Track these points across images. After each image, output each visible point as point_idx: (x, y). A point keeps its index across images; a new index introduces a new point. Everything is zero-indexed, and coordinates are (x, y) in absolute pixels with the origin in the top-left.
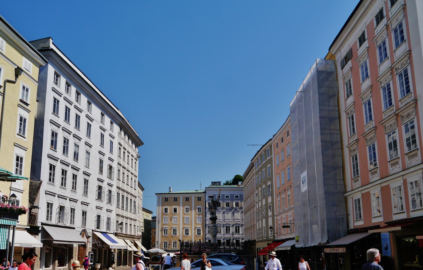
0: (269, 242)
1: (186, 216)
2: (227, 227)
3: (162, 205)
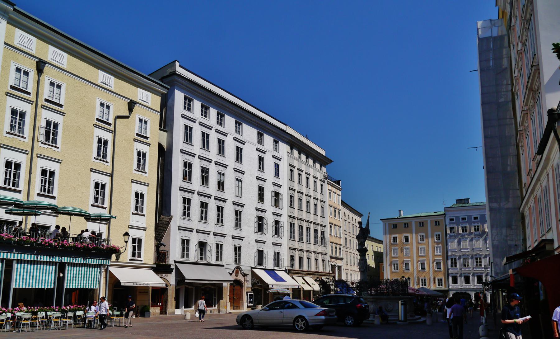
1: (420, 246)
2: (477, 259)
3: (390, 234)
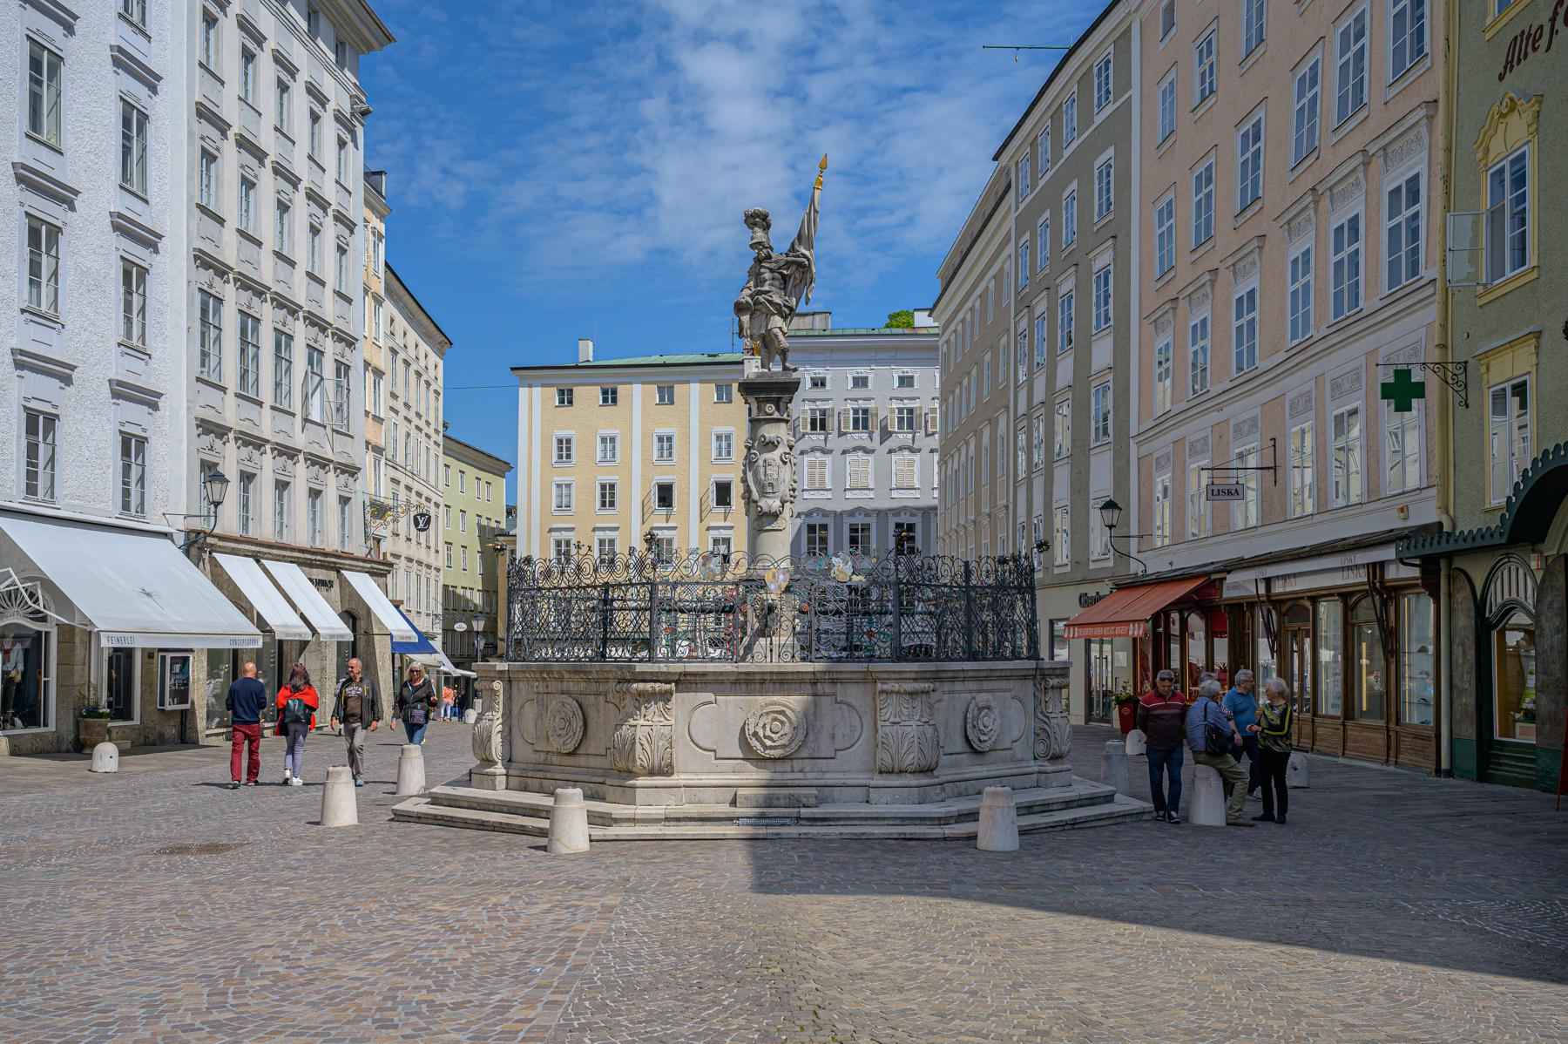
0: (1091, 590)
